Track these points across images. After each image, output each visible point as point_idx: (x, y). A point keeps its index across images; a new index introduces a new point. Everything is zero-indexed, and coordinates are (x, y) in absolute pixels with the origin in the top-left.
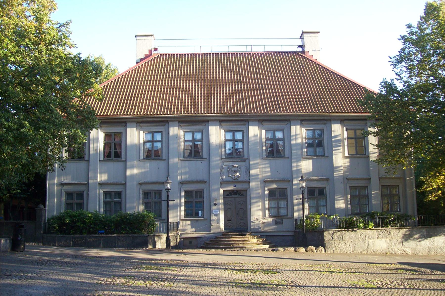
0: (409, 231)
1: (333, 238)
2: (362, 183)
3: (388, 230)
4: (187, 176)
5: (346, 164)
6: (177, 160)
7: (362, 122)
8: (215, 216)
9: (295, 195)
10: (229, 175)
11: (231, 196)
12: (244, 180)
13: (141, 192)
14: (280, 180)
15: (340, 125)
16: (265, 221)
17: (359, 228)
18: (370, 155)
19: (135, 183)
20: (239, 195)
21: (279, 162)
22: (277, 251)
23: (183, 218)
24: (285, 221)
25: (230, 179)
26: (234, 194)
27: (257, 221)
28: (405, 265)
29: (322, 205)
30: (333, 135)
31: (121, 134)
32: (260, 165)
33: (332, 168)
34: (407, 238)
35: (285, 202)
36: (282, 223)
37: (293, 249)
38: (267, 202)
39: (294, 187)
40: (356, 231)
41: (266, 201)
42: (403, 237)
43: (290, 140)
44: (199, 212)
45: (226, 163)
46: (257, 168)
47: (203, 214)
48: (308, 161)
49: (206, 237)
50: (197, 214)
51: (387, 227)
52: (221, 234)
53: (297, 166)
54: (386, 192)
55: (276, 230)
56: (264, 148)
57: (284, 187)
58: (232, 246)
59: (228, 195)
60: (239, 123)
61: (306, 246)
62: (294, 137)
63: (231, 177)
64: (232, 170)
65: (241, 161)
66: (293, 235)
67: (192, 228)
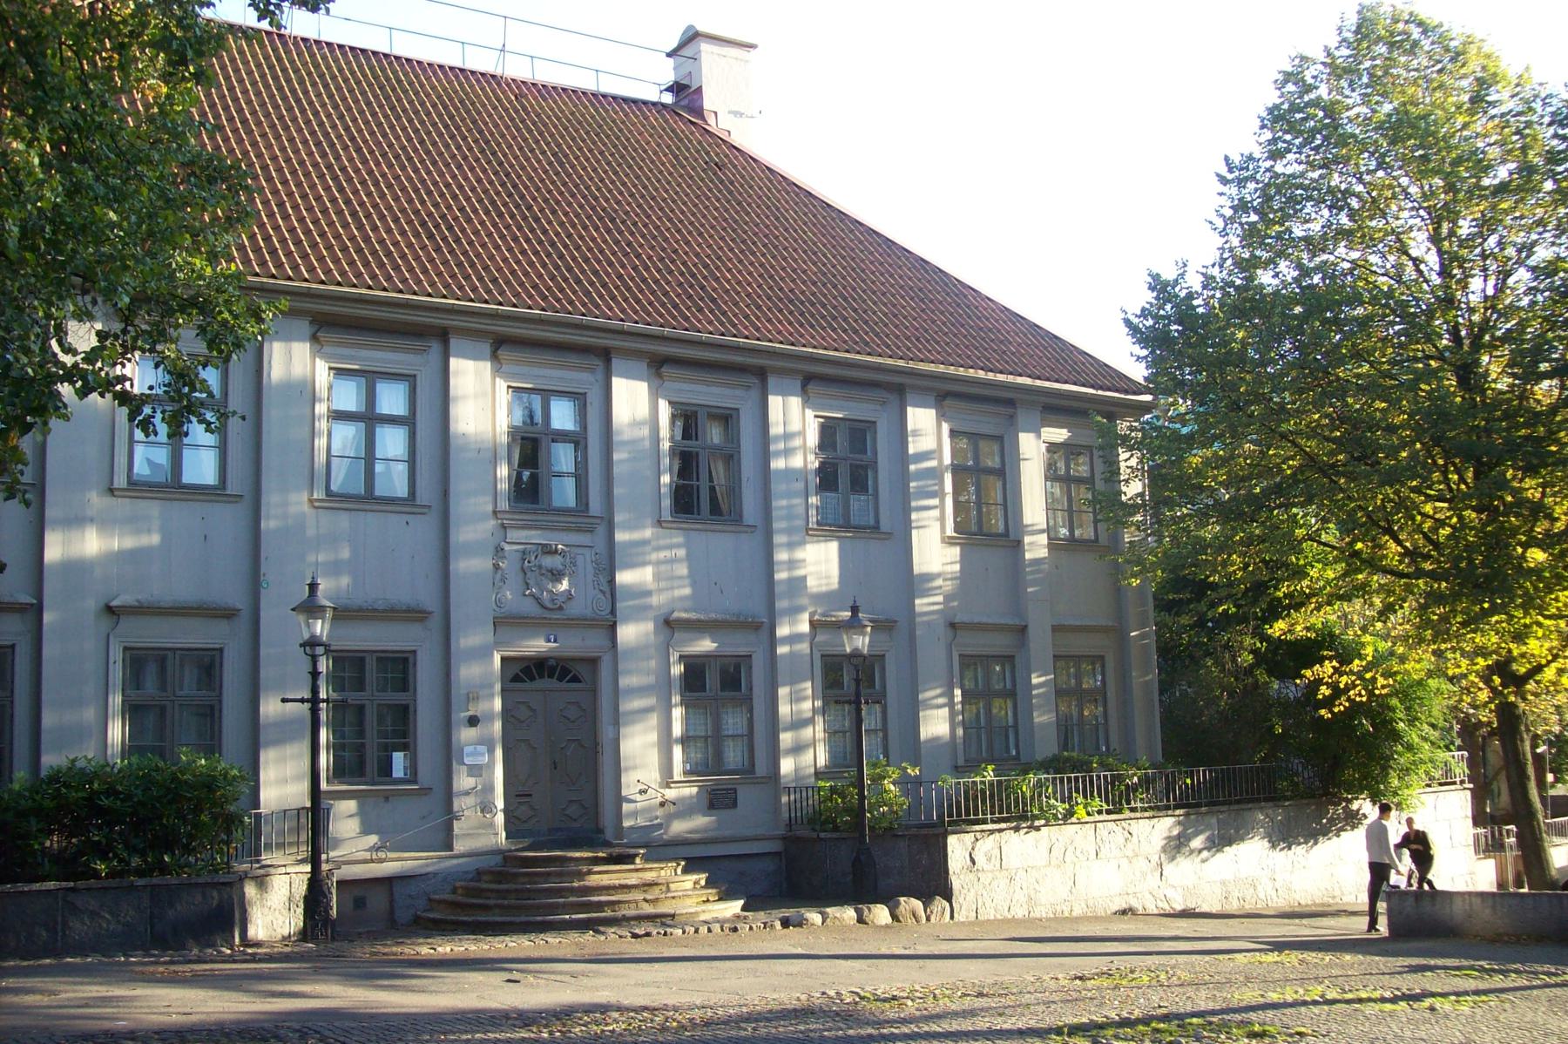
0: (1179, 823)
1: (973, 862)
2: (998, 644)
4: (345, 581)
5: (949, 568)
6: (299, 502)
7: (1002, 410)
8: (469, 775)
9: (784, 685)
10: (528, 586)
11: (528, 685)
12: (588, 612)
13: (117, 654)
14: (720, 617)
15: (933, 412)
16: (671, 794)
17: (1052, 820)
18: (1027, 539)
19: (92, 604)
20: (560, 679)
21: (720, 543)
22: (800, 925)
24: (745, 795)
25: (529, 607)
26: (541, 676)
27: (644, 797)
28: (1320, 950)
29: (730, 733)
30: (911, 451)
32: (659, 549)
33: (911, 584)
34: (1176, 845)
36: (734, 804)
37: (849, 914)
38: (677, 713)
39: (782, 650)
40: (1038, 829)
41: (676, 705)
42: (1164, 849)
43: (765, 456)
45: (513, 535)
46: (644, 564)
47: (413, 768)
48: (823, 545)
49: (435, 874)
50: (386, 769)
51: (1120, 811)
52: (499, 858)
53: (792, 564)
55: (710, 834)
56: (666, 479)
57: (742, 651)
58: (608, 913)
59: (516, 679)
60: (548, 356)
61: (889, 899)
62: (781, 446)
63: (537, 599)
64: (540, 567)
65: (579, 530)
66: (776, 853)
67: (366, 830)
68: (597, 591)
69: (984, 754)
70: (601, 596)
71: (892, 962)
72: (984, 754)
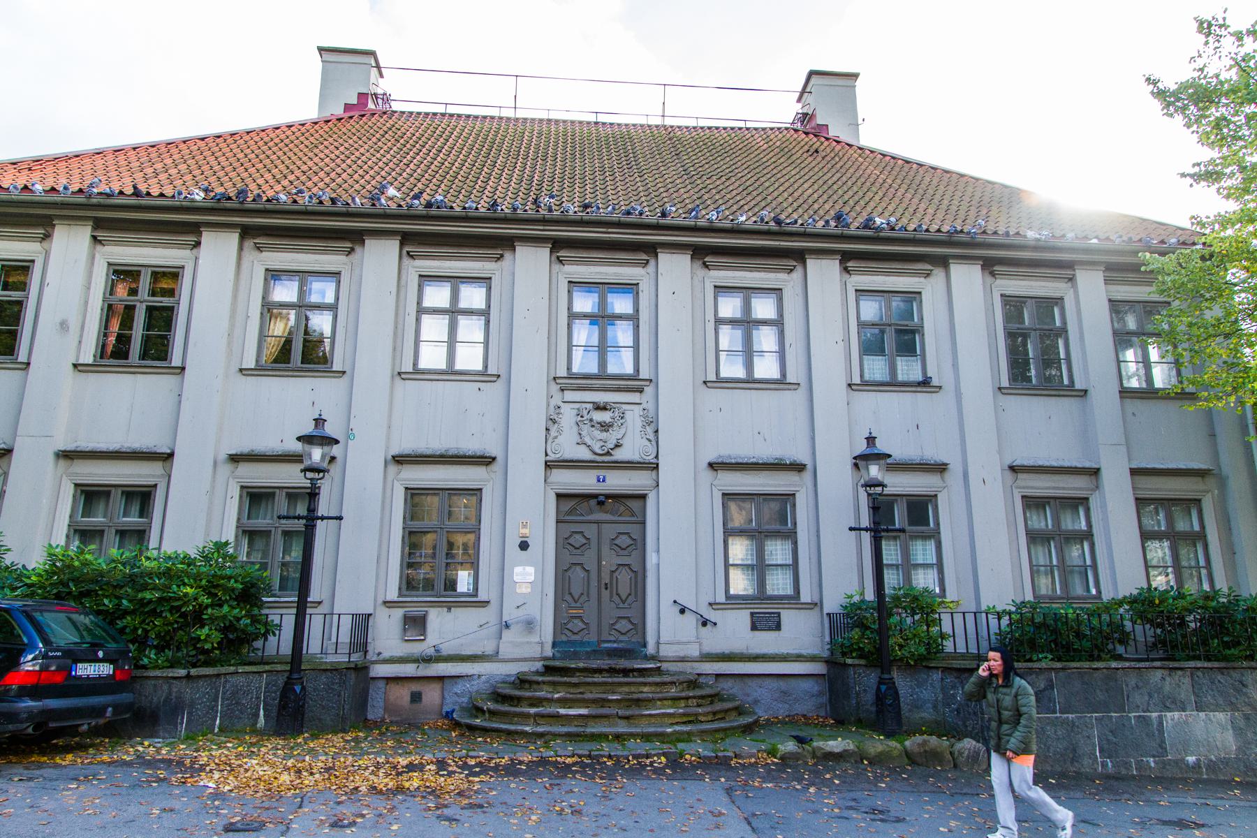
3: (1235, 675)
23: (393, 595)
31: (174, 274)
35: (788, 545)
36: (778, 627)
44: (460, 573)
45: (569, 395)
50: (451, 585)
54: (1042, 522)
64: (591, 420)
68: (644, 440)
69: (1058, 592)
70: (648, 443)
71: (38, 337)
72: (1058, 592)
